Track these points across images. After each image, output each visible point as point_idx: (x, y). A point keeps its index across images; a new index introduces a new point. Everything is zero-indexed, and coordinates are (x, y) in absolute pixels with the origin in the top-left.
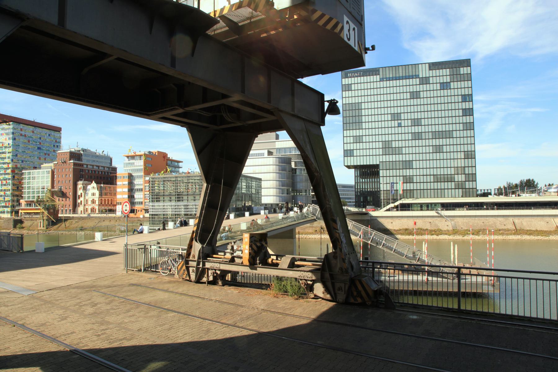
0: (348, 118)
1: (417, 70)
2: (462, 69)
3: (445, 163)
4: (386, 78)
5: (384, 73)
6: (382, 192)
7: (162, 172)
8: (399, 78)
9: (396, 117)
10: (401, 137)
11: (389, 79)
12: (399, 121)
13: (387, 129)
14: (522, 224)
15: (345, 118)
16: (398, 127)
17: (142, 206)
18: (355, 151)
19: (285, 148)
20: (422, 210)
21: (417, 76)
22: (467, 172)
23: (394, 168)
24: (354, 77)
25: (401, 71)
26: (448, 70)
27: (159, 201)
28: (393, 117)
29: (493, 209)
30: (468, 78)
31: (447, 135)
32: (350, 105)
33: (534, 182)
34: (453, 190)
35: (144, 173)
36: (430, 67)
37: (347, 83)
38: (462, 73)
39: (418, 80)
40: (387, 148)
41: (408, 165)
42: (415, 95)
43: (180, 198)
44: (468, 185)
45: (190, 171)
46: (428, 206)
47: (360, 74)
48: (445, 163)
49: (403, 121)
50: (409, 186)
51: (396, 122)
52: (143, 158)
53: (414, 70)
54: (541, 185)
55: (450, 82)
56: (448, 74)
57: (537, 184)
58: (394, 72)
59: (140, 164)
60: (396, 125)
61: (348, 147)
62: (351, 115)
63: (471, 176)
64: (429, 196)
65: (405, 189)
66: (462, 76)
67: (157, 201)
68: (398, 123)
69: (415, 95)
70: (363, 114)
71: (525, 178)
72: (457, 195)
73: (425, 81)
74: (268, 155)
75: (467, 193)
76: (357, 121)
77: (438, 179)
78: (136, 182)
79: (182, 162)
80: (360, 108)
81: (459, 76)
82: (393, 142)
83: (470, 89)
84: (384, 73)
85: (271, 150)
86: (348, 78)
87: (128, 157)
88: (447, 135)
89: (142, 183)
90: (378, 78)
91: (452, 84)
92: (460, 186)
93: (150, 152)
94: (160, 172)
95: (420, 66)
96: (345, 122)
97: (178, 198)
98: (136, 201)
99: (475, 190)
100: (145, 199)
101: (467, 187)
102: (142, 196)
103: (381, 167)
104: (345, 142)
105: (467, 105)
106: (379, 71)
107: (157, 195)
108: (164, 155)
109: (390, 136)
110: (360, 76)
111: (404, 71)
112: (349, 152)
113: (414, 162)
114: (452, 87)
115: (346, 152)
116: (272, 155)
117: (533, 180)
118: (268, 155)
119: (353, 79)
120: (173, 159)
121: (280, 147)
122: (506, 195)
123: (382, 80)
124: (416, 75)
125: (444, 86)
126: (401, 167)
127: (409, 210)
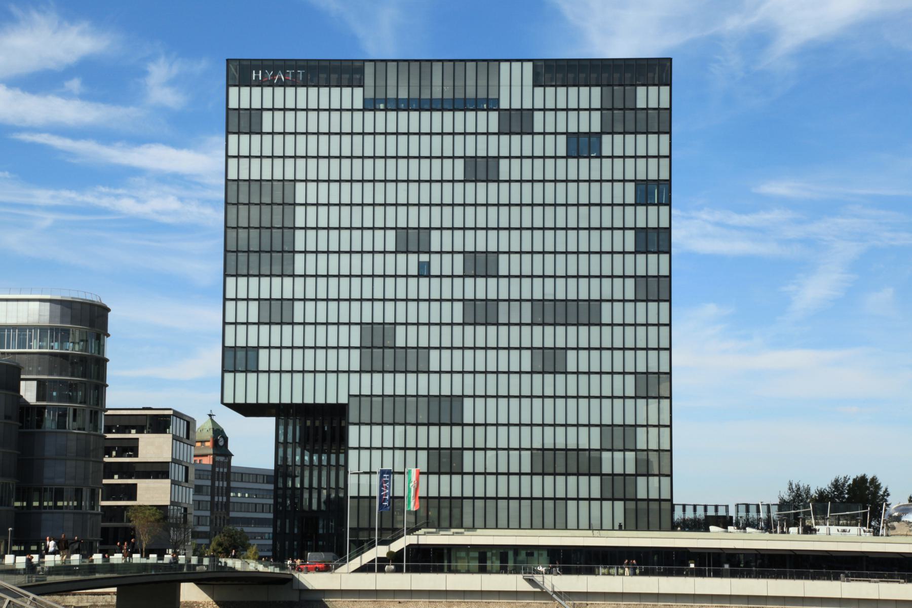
2: (641, 91)
3: (571, 411)
4: (386, 100)
9: (412, 241)
11: (397, 106)
12: (424, 258)
16: (419, 276)
20: (483, 570)
21: (491, 105)
31: (583, 313)
40: (379, 347)
41: (446, 411)
42: (481, 170)
46: (504, 558)
47: (295, 75)
48: (571, 411)
49: (435, 258)
53: (482, 82)
55: (599, 135)
60: (413, 271)
66: (641, 116)
68: (420, 264)
69: (481, 170)
73: (517, 122)
76: (277, 246)
77: (548, 461)
88: (583, 313)
92: (617, 488)
103: (353, 416)
106: (361, 71)
117: (874, 480)
123: (370, 105)
125: (582, 146)
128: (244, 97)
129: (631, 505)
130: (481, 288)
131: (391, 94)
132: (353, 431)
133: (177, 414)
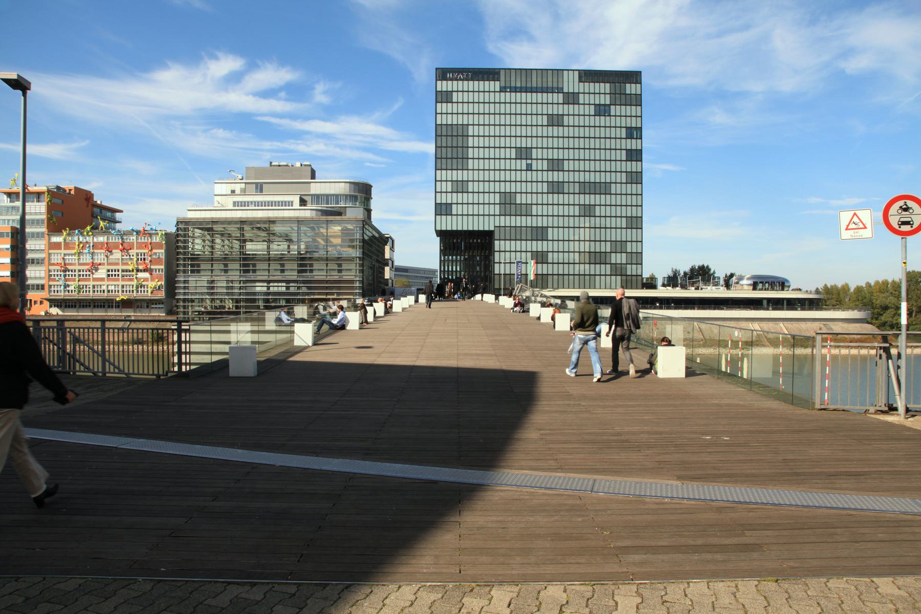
0: (444, 150)
1: (560, 80)
2: (628, 86)
4: (510, 87)
5: (508, 79)
6: (497, 277)
7: (89, 228)
8: (531, 90)
9: (524, 153)
10: (530, 186)
11: (515, 90)
12: (529, 162)
13: (497, 172)
14: (712, 331)
15: (439, 150)
16: (527, 170)
17: (44, 294)
18: (454, 207)
19: (327, 196)
21: (560, 90)
22: (629, 250)
23: (524, 238)
24: (456, 80)
25: (534, 79)
26: (608, 85)
27: (199, 271)
28: (519, 153)
29: (668, 308)
30: (637, 100)
31: (602, 188)
32: (449, 127)
33: (710, 270)
34: (608, 277)
35: (48, 228)
36: (580, 77)
37: (444, 89)
38: (628, 92)
39: (561, 95)
40: (508, 204)
41: (540, 233)
42: (555, 121)
43: (248, 265)
44: (631, 270)
45: (148, 228)
49: (534, 162)
50: (544, 269)
51: (524, 162)
52: (46, 198)
53: (555, 80)
54: (720, 272)
56: (608, 91)
57: (714, 272)
58: (524, 79)
59: (38, 210)
60: (524, 167)
61: (443, 199)
62: (449, 145)
63: (634, 255)
64: (571, 285)
65: (540, 272)
66: (628, 97)
67: (192, 271)
69: (555, 121)
70: (470, 145)
71: (697, 263)
72: (613, 285)
73: (572, 99)
74: (301, 205)
75: (629, 282)
78: (30, 245)
79: (121, 211)
80: (465, 134)
81: (623, 97)
82: (518, 196)
83: (639, 119)
84: (508, 79)
85: (304, 197)
86: (446, 80)
87: (9, 195)
88: (602, 188)
89: (43, 247)
90: (495, 85)
91: (612, 107)
92: (618, 270)
93: (58, 188)
94: (84, 228)
95: (565, 73)
96: (439, 156)
97: (244, 265)
98: (29, 282)
99: (639, 278)
100: (50, 280)
101: (629, 273)
102: (43, 274)
103: (497, 236)
104: (439, 190)
105: (632, 144)
107: (192, 259)
108: (87, 197)
109: (582, 173)
110: (468, 80)
111: (539, 79)
112: (444, 207)
113: (550, 230)
114: (613, 113)
115: (439, 207)
116: (305, 205)
118: (301, 205)
119: (455, 82)
120: (105, 204)
121: (318, 192)
122: (684, 287)
123: (503, 90)
124: (558, 88)
125: (602, 110)
126: (513, 238)
127: (821, 309)
128: (444, 86)
129: (624, 278)
130: (556, 176)
131: (513, 85)
132: (497, 243)
133: (390, 238)
